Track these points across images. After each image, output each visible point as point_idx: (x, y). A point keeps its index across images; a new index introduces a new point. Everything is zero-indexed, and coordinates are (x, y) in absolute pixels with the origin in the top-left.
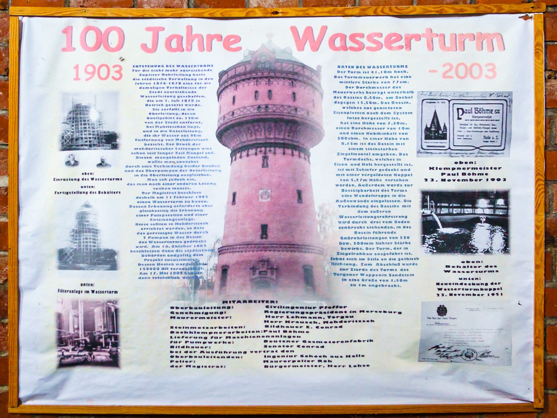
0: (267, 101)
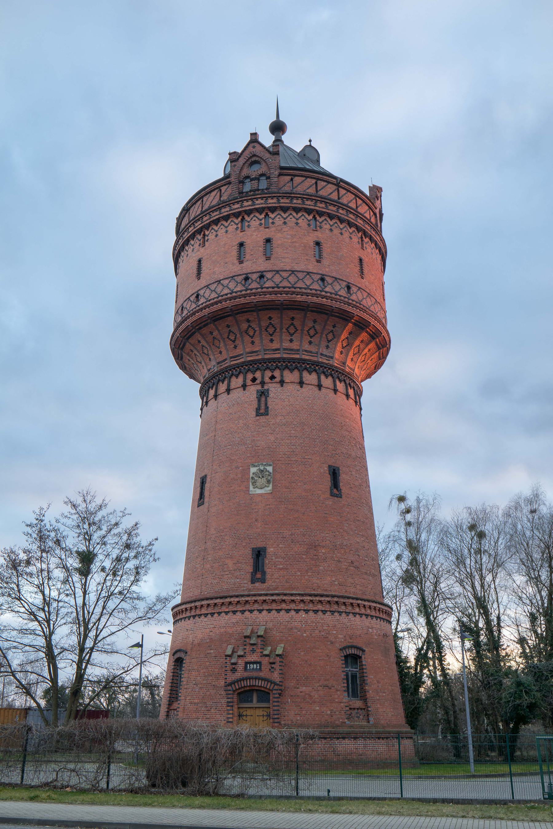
0: (262, 265)
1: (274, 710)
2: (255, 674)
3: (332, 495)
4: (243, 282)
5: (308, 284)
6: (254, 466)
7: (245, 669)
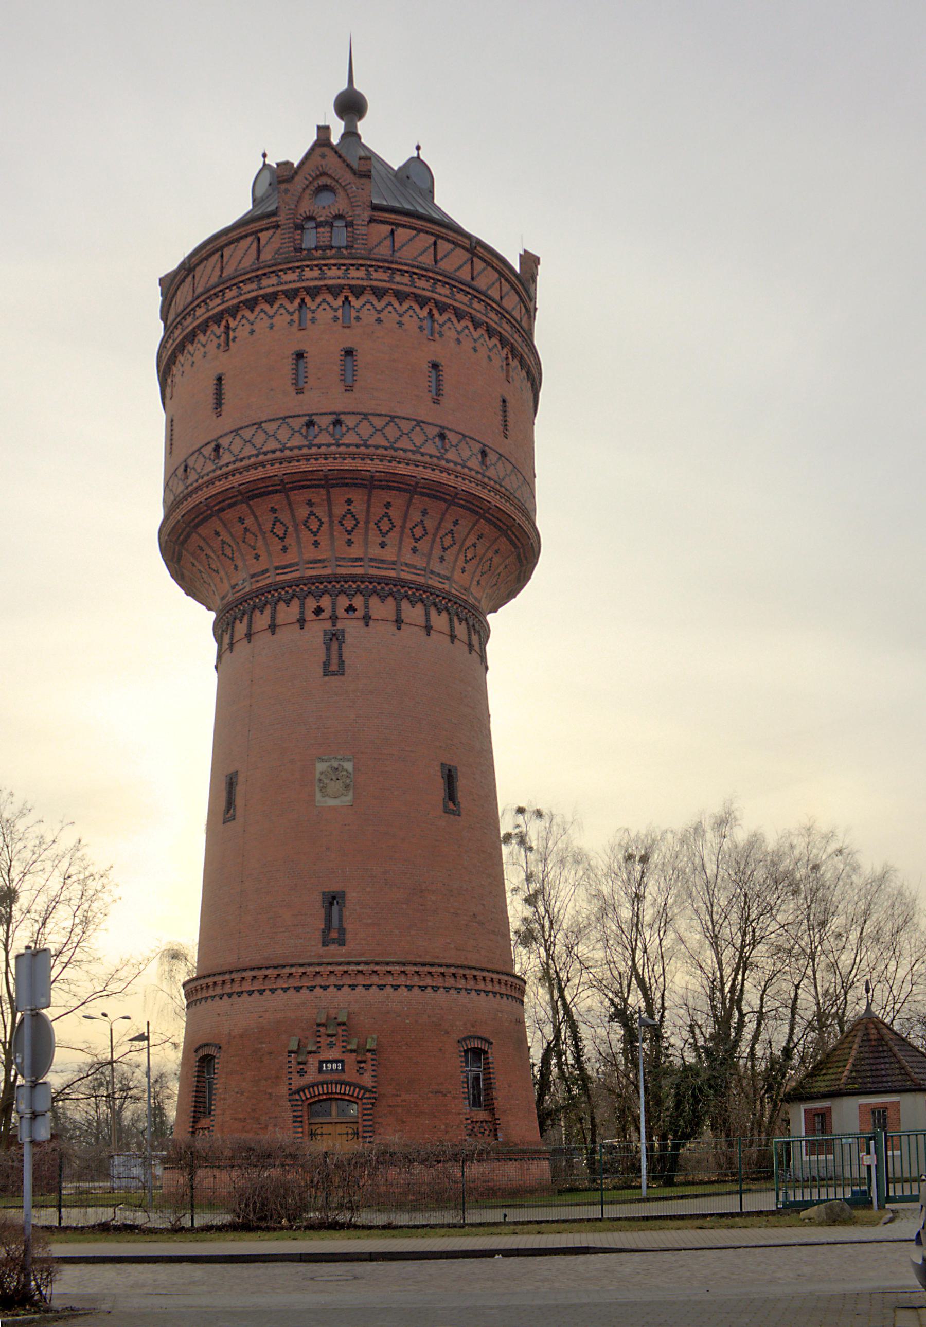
0: (338, 401)
1: (364, 1126)
2: (335, 1077)
3: (447, 811)
4: (304, 431)
5: (418, 444)
6: (323, 760)
7: (320, 1070)
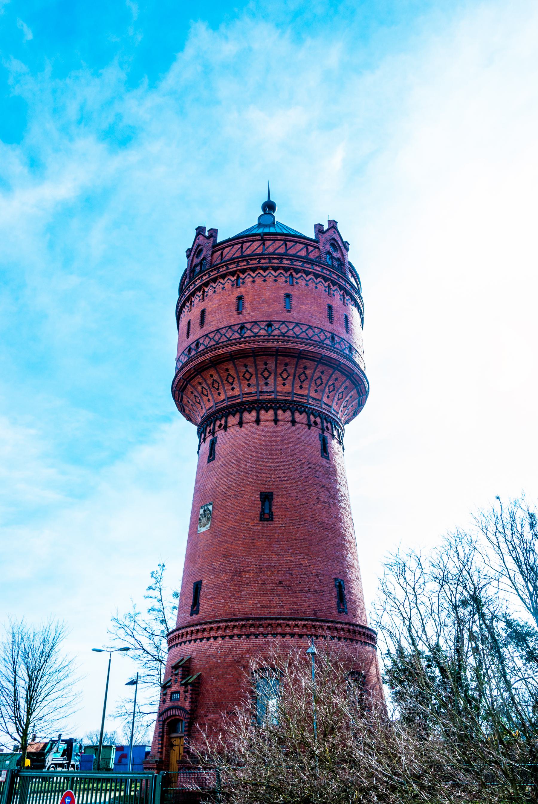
5: (229, 337)
